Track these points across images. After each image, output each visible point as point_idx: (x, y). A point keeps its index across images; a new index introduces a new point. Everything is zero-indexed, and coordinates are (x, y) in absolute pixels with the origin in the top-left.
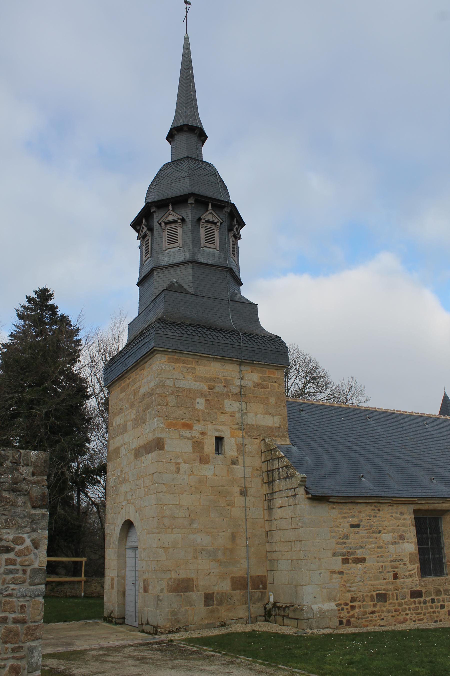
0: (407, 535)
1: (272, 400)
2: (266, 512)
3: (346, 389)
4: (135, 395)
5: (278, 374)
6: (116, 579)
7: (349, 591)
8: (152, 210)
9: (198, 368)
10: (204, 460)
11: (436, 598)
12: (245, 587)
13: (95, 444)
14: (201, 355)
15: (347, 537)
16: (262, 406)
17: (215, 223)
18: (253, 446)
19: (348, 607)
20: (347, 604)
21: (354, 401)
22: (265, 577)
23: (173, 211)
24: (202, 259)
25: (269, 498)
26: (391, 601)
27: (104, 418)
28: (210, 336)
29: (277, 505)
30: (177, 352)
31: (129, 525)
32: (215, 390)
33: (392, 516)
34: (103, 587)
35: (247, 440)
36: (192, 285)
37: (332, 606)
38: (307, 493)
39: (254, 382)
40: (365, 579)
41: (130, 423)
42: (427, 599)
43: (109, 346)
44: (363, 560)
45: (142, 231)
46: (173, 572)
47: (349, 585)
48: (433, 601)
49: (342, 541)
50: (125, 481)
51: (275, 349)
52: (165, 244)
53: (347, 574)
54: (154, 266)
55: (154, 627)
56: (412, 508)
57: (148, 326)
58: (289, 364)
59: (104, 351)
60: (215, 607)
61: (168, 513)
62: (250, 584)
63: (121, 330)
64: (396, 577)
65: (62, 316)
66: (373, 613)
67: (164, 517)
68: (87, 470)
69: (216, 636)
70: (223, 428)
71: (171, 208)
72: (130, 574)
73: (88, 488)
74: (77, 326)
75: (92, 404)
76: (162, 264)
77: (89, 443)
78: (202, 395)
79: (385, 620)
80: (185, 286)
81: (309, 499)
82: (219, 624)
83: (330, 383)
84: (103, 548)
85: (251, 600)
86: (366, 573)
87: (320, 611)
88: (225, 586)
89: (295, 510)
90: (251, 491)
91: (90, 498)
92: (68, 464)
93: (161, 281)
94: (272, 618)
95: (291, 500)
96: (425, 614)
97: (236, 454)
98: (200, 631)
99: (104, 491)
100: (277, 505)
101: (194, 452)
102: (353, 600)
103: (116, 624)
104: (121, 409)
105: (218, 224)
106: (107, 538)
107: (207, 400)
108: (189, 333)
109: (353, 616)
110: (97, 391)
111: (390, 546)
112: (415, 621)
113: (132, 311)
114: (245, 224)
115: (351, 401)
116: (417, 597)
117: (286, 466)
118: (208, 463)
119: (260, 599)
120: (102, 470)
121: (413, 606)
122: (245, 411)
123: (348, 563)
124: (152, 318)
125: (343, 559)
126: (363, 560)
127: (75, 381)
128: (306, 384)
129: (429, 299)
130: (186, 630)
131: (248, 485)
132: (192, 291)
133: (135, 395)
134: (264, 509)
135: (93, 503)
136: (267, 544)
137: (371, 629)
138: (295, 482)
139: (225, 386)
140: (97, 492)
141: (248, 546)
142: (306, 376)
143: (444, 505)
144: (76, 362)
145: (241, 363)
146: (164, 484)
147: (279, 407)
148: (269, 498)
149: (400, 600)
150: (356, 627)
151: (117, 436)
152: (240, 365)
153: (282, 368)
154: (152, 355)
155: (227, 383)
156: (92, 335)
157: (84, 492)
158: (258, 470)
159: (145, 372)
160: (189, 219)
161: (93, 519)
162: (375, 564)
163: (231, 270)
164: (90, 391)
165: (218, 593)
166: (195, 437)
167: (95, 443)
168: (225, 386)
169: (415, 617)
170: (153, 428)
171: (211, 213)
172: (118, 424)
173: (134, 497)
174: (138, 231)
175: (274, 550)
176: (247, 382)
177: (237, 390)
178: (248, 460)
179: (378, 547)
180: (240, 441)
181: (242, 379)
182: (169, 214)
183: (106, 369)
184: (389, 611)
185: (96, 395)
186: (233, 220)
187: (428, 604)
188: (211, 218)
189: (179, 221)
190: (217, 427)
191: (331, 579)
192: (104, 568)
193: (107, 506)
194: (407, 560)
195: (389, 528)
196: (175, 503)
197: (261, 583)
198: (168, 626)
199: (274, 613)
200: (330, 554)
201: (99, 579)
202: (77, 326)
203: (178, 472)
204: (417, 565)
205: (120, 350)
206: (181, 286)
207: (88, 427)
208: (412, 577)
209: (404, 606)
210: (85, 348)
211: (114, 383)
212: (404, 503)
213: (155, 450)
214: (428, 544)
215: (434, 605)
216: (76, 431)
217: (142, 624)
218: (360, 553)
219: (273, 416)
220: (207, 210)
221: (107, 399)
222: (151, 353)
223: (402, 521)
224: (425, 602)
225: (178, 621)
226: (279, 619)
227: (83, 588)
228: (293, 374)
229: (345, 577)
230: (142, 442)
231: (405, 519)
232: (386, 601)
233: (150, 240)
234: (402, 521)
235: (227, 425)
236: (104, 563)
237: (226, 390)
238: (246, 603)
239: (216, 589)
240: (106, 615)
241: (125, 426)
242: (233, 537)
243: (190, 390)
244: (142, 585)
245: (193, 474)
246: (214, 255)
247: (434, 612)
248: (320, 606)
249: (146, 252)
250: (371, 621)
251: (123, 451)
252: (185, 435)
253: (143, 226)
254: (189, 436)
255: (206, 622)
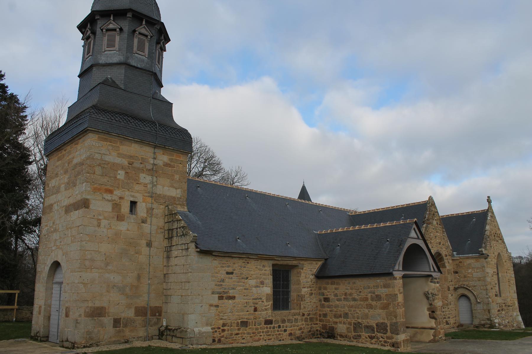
0: (266, 281)
1: (177, 177)
2: (165, 260)
3: (233, 175)
4: (69, 163)
5: (182, 158)
6: (43, 307)
7: (221, 319)
8: (96, 18)
9: (121, 147)
10: (120, 218)
11: (281, 325)
12: (145, 314)
13: (33, 200)
14: (126, 136)
15: (223, 281)
16: (169, 180)
17: (146, 36)
18: (160, 210)
19: (220, 330)
20: (219, 328)
21: (238, 184)
22: (161, 307)
23: (114, 21)
24: (133, 63)
25: (168, 250)
26: (250, 327)
27: (42, 181)
28: (133, 124)
29: (174, 255)
30: (106, 133)
31: (56, 265)
32: (133, 165)
33: (257, 268)
34: (32, 313)
35: (155, 206)
36: (123, 82)
37: (209, 329)
38: (197, 247)
39: (164, 162)
40: (233, 311)
41: (63, 186)
42: (276, 325)
43: (50, 124)
44: (233, 298)
45: (86, 34)
46: (90, 302)
47: (222, 315)
48: (279, 327)
49: (219, 283)
50: (56, 231)
51: (183, 139)
52: (105, 47)
53: (221, 307)
54: (94, 63)
55: (72, 343)
56: (271, 262)
57: (84, 111)
58: (192, 151)
59: (46, 127)
60: (121, 328)
61: (89, 257)
62: (149, 312)
63: (62, 112)
64: (255, 310)
65: (12, 95)
66: (237, 334)
67: (86, 260)
68: (25, 222)
69: (120, 350)
70: (137, 195)
71: (112, 18)
72: (55, 303)
73: (24, 236)
74: (25, 105)
75: (33, 169)
76: (101, 62)
77: (28, 200)
78: (123, 168)
79: (245, 340)
80: (117, 82)
81: (197, 252)
82: (123, 341)
83: (222, 169)
84: (33, 283)
85: (149, 324)
86: (234, 306)
87: (199, 332)
88: (130, 313)
89: (186, 260)
90: (155, 244)
91: (26, 244)
92: (8, 215)
93: (98, 76)
94: (164, 337)
95: (184, 252)
96: (273, 335)
97: (145, 215)
98: (109, 346)
99: (38, 239)
100: (174, 255)
101: (113, 212)
102: (224, 325)
103: (41, 341)
104: (57, 174)
105: (149, 37)
106: (38, 275)
107: (126, 173)
108: (116, 119)
109: (223, 336)
110: (38, 159)
111: (254, 288)
112: (265, 340)
113: (73, 98)
114: (170, 40)
115: (236, 184)
116: (268, 324)
117: (183, 227)
118: (123, 220)
119: (156, 324)
120: (38, 222)
121: (266, 330)
122: (155, 183)
123: (223, 299)
124: (87, 105)
125: (219, 296)
126: (233, 298)
127: (19, 149)
128: (204, 168)
129: (295, 114)
130: (97, 345)
131: (152, 240)
132: (122, 86)
133: (69, 163)
134: (163, 258)
135: (29, 248)
136: (164, 284)
137: (234, 345)
138: (188, 239)
139: (141, 163)
140: (33, 240)
141: (149, 284)
142: (205, 162)
143: (294, 262)
144: (21, 133)
145: (155, 147)
146: (87, 235)
147: (182, 182)
148: (168, 250)
149: (257, 326)
150: (224, 344)
151: (52, 195)
152: (155, 148)
153: (187, 154)
154: (86, 133)
155: (143, 161)
156: (37, 113)
157: (21, 239)
158: (161, 228)
159: (79, 147)
160: (126, 29)
161: (28, 260)
162: (242, 301)
163: (155, 74)
164: (32, 158)
165: (124, 319)
166: (115, 200)
167: (33, 201)
168: (141, 163)
169: (266, 337)
170: (83, 190)
171: (144, 27)
172: (53, 185)
173: (62, 243)
174: (83, 33)
175: (169, 288)
176: (158, 162)
177: (150, 167)
178: (154, 220)
179: (245, 289)
180: (149, 205)
181: (155, 158)
182: (110, 23)
183: (46, 141)
184: (248, 333)
185: (37, 162)
186: (161, 37)
187: (276, 329)
188: (143, 31)
189: (118, 30)
190: (133, 194)
191: (209, 310)
192: (33, 298)
193: (39, 250)
194: (264, 299)
195: (254, 276)
196: (95, 249)
197: (157, 312)
198: (83, 342)
199: (165, 334)
200: (210, 292)
201: (29, 307)
202: (25, 105)
203: (99, 226)
204: (271, 303)
205: (60, 126)
206: (114, 82)
207: (28, 187)
208: (266, 310)
209: (260, 330)
210: (30, 123)
211: (52, 153)
212: (266, 259)
213: (82, 208)
214: (280, 288)
215: (279, 329)
216: (18, 189)
217: (62, 341)
218: (231, 293)
219: (176, 189)
220: (141, 25)
221: (46, 166)
222: (85, 132)
223: (263, 272)
224: (274, 328)
225: (91, 338)
226: (169, 338)
227: (15, 314)
228: (195, 160)
229: (220, 309)
230: (72, 201)
231: (265, 270)
232: (247, 327)
233: (92, 41)
234: (263, 272)
235: (140, 193)
236: (34, 295)
237: (142, 166)
238: (145, 327)
239: (123, 315)
240: (32, 334)
241: (59, 187)
242: (139, 277)
243: (114, 164)
244: (64, 312)
245: (111, 228)
246: (143, 61)
247: (280, 334)
248: (200, 329)
249: (88, 50)
250: (235, 340)
251: (55, 207)
252: (106, 198)
253: (87, 29)
254: (110, 198)
255: (114, 339)
